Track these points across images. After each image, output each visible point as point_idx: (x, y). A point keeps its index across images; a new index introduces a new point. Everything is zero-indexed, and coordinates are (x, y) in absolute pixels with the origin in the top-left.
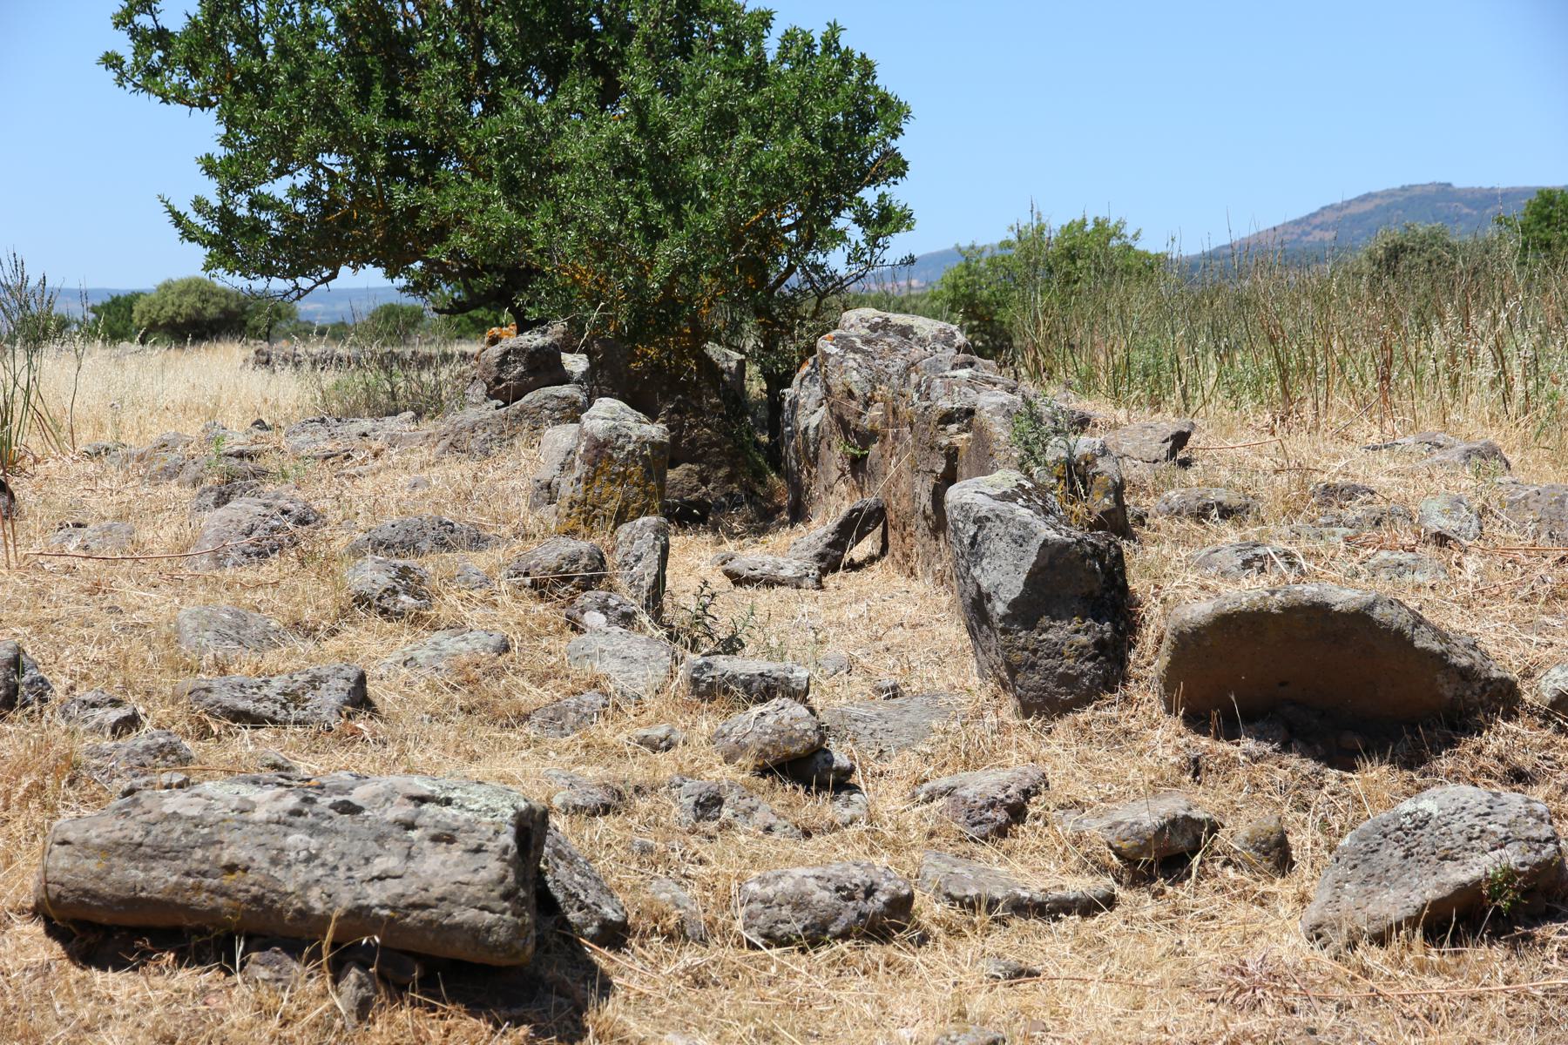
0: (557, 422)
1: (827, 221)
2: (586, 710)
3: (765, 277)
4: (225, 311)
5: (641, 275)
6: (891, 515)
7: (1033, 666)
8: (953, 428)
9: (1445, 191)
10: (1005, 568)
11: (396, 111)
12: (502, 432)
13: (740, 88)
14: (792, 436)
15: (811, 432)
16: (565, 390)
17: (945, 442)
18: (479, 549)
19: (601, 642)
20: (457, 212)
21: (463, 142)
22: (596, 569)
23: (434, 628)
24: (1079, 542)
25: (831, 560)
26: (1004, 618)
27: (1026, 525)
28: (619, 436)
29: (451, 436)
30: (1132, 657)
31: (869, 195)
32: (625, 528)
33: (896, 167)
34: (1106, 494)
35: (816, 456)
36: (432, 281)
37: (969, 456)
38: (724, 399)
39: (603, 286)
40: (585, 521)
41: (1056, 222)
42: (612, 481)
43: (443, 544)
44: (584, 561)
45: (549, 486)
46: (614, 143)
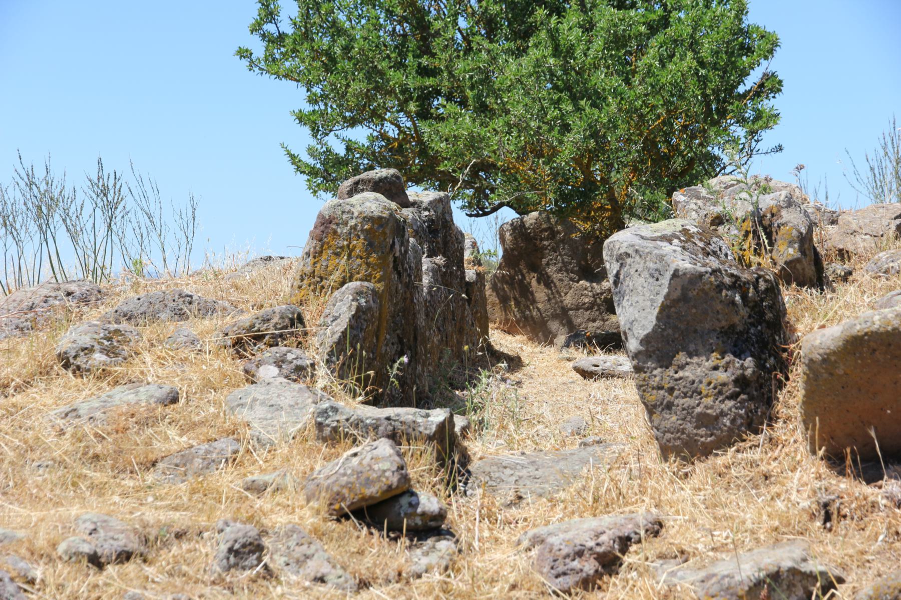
2: (214, 456)
7: (669, 406)
10: (641, 304)
24: (714, 272)
34: (791, 243)
42: (337, 255)
43: (181, 315)
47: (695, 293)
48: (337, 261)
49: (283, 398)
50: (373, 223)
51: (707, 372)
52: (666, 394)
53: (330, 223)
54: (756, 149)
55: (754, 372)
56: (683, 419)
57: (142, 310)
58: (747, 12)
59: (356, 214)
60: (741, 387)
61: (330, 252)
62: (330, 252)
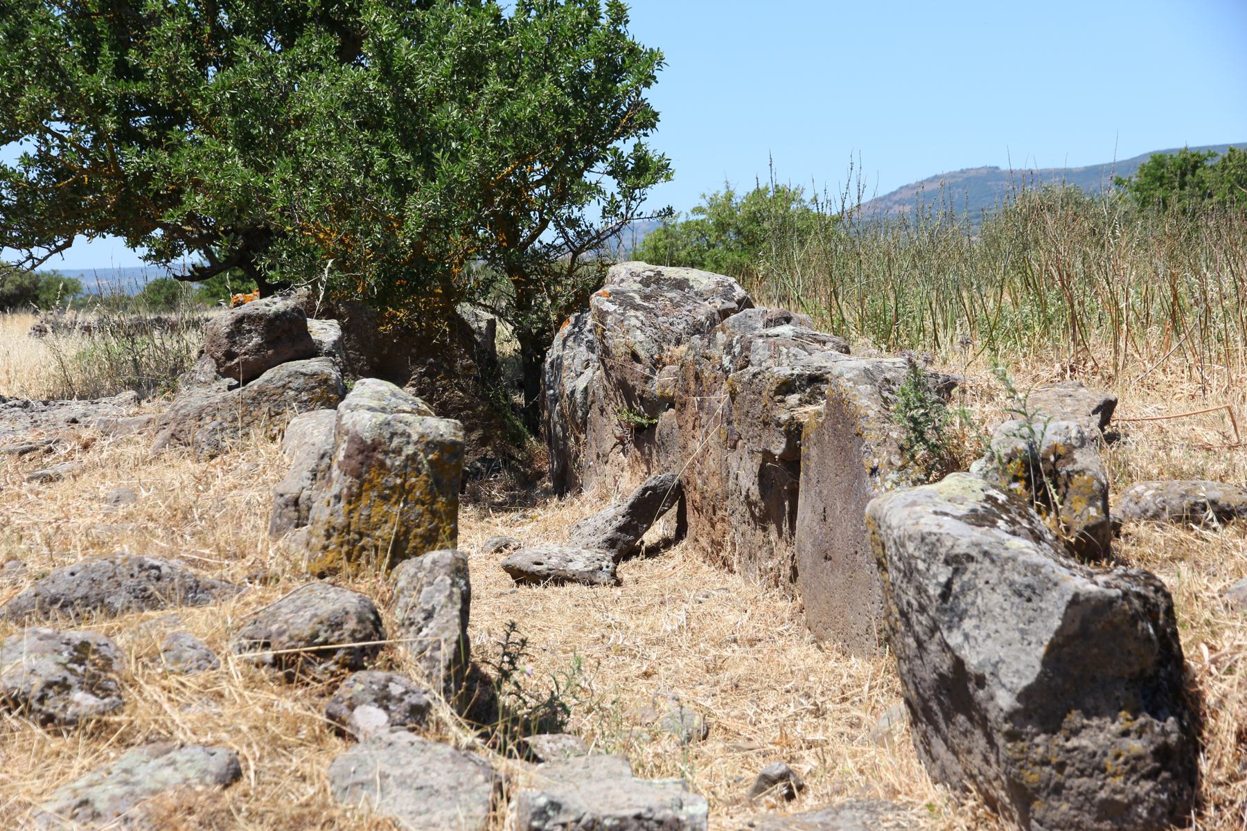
0: (306, 406)
1: (579, 174)
3: (517, 234)
4: (19, 287)
5: (389, 232)
6: (692, 496)
7: (1058, 790)
8: (793, 399)
9: (994, 172)
11: (123, 71)
12: (235, 419)
13: (490, 30)
14: (556, 399)
15: (578, 396)
16: (313, 365)
17: (785, 417)
18: (195, 603)
19: (379, 761)
20: (192, 174)
21: (197, 103)
22: (367, 637)
23: (124, 742)
25: (625, 544)
26: (1011, 716)
27: (1036, 569)
28: (393, 435)
29: (173, 426)
30: (1204, 766)
31: (626, 146)
32: (407, 568)
33: (649, 120)
35: (585, 423)
36: (174, 248)
37: (820, 435)
38: (479, 362)
39: (349, 246)
40: (349, 555)
41: (743, 190)
42: (385, 499)
43: (146, 600)
44: (351, 625)
45: (296, 502)
46: (356, 89)
47: (1099, 627)
48: (385, 508)
49: (434, 775)
50: (442, 451)
51: (1114, 739)
52: (1054, 772)
53: (374, 450)
54: (638, 212)
55: (1179, 738)
56: (1080, 809)
57: (81, 592)
58: (627, 21)
59: (415, 437)
60: (1161, 761)
61: (373, 494)
62: (373, 494)
